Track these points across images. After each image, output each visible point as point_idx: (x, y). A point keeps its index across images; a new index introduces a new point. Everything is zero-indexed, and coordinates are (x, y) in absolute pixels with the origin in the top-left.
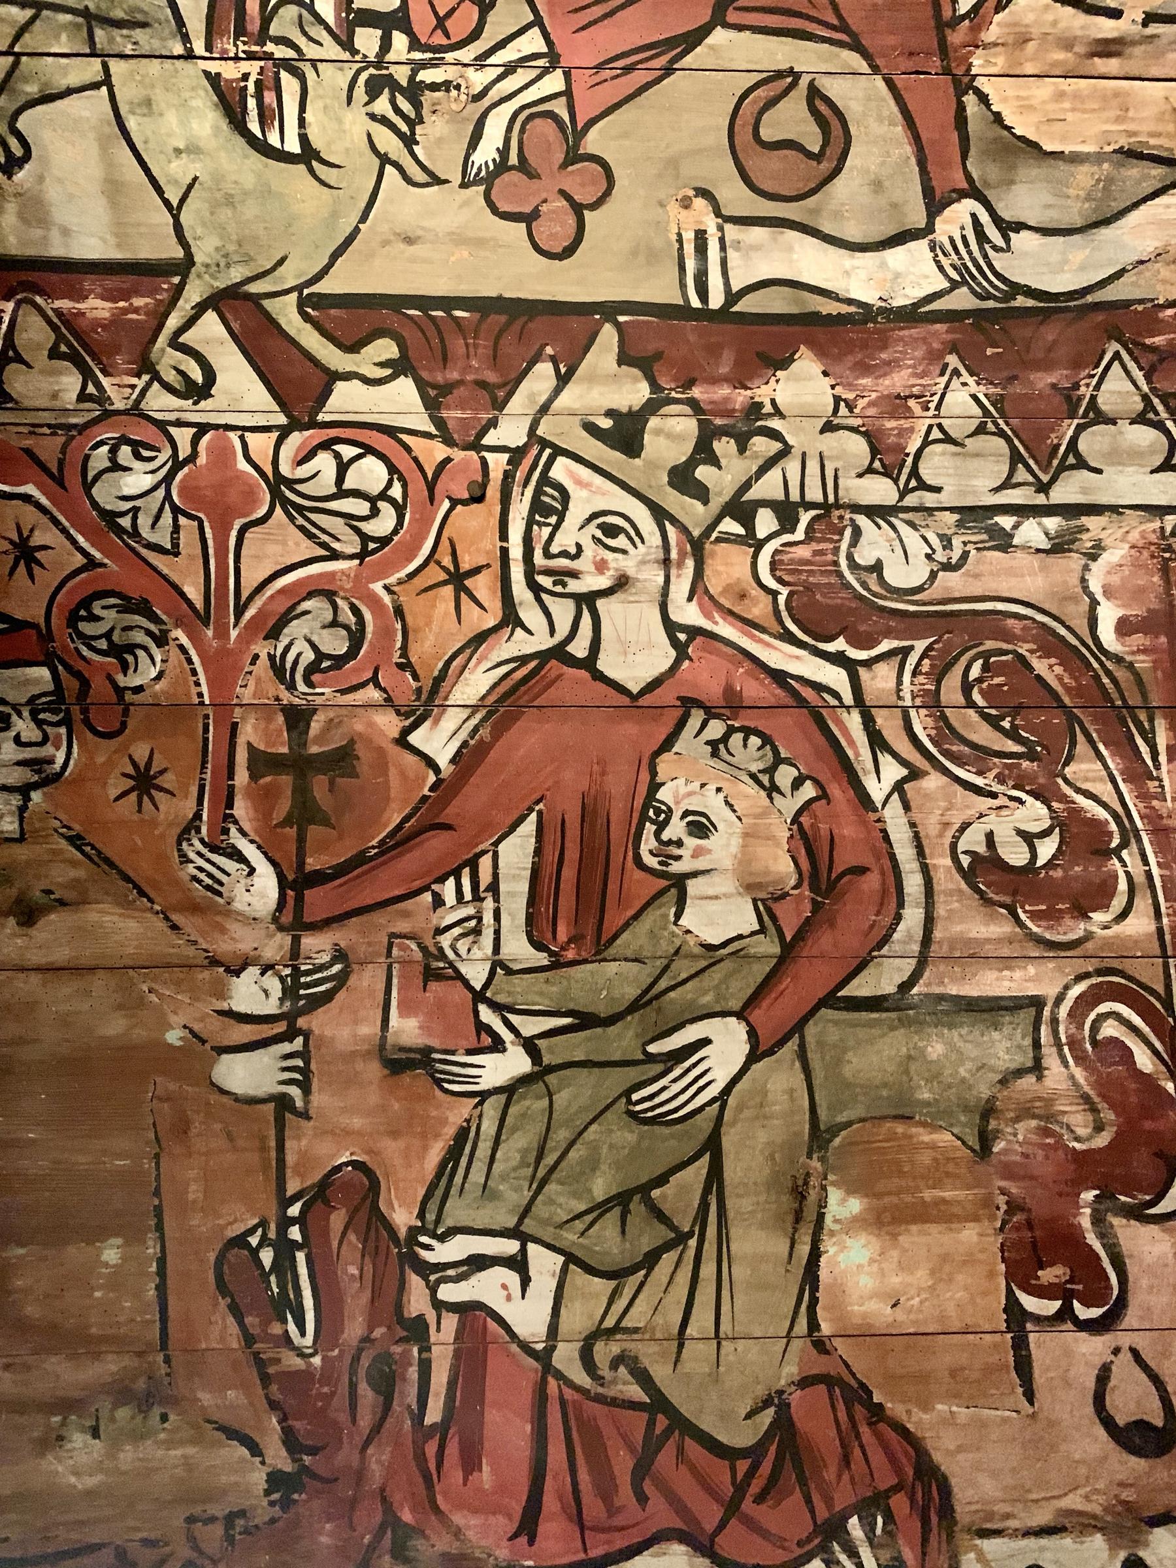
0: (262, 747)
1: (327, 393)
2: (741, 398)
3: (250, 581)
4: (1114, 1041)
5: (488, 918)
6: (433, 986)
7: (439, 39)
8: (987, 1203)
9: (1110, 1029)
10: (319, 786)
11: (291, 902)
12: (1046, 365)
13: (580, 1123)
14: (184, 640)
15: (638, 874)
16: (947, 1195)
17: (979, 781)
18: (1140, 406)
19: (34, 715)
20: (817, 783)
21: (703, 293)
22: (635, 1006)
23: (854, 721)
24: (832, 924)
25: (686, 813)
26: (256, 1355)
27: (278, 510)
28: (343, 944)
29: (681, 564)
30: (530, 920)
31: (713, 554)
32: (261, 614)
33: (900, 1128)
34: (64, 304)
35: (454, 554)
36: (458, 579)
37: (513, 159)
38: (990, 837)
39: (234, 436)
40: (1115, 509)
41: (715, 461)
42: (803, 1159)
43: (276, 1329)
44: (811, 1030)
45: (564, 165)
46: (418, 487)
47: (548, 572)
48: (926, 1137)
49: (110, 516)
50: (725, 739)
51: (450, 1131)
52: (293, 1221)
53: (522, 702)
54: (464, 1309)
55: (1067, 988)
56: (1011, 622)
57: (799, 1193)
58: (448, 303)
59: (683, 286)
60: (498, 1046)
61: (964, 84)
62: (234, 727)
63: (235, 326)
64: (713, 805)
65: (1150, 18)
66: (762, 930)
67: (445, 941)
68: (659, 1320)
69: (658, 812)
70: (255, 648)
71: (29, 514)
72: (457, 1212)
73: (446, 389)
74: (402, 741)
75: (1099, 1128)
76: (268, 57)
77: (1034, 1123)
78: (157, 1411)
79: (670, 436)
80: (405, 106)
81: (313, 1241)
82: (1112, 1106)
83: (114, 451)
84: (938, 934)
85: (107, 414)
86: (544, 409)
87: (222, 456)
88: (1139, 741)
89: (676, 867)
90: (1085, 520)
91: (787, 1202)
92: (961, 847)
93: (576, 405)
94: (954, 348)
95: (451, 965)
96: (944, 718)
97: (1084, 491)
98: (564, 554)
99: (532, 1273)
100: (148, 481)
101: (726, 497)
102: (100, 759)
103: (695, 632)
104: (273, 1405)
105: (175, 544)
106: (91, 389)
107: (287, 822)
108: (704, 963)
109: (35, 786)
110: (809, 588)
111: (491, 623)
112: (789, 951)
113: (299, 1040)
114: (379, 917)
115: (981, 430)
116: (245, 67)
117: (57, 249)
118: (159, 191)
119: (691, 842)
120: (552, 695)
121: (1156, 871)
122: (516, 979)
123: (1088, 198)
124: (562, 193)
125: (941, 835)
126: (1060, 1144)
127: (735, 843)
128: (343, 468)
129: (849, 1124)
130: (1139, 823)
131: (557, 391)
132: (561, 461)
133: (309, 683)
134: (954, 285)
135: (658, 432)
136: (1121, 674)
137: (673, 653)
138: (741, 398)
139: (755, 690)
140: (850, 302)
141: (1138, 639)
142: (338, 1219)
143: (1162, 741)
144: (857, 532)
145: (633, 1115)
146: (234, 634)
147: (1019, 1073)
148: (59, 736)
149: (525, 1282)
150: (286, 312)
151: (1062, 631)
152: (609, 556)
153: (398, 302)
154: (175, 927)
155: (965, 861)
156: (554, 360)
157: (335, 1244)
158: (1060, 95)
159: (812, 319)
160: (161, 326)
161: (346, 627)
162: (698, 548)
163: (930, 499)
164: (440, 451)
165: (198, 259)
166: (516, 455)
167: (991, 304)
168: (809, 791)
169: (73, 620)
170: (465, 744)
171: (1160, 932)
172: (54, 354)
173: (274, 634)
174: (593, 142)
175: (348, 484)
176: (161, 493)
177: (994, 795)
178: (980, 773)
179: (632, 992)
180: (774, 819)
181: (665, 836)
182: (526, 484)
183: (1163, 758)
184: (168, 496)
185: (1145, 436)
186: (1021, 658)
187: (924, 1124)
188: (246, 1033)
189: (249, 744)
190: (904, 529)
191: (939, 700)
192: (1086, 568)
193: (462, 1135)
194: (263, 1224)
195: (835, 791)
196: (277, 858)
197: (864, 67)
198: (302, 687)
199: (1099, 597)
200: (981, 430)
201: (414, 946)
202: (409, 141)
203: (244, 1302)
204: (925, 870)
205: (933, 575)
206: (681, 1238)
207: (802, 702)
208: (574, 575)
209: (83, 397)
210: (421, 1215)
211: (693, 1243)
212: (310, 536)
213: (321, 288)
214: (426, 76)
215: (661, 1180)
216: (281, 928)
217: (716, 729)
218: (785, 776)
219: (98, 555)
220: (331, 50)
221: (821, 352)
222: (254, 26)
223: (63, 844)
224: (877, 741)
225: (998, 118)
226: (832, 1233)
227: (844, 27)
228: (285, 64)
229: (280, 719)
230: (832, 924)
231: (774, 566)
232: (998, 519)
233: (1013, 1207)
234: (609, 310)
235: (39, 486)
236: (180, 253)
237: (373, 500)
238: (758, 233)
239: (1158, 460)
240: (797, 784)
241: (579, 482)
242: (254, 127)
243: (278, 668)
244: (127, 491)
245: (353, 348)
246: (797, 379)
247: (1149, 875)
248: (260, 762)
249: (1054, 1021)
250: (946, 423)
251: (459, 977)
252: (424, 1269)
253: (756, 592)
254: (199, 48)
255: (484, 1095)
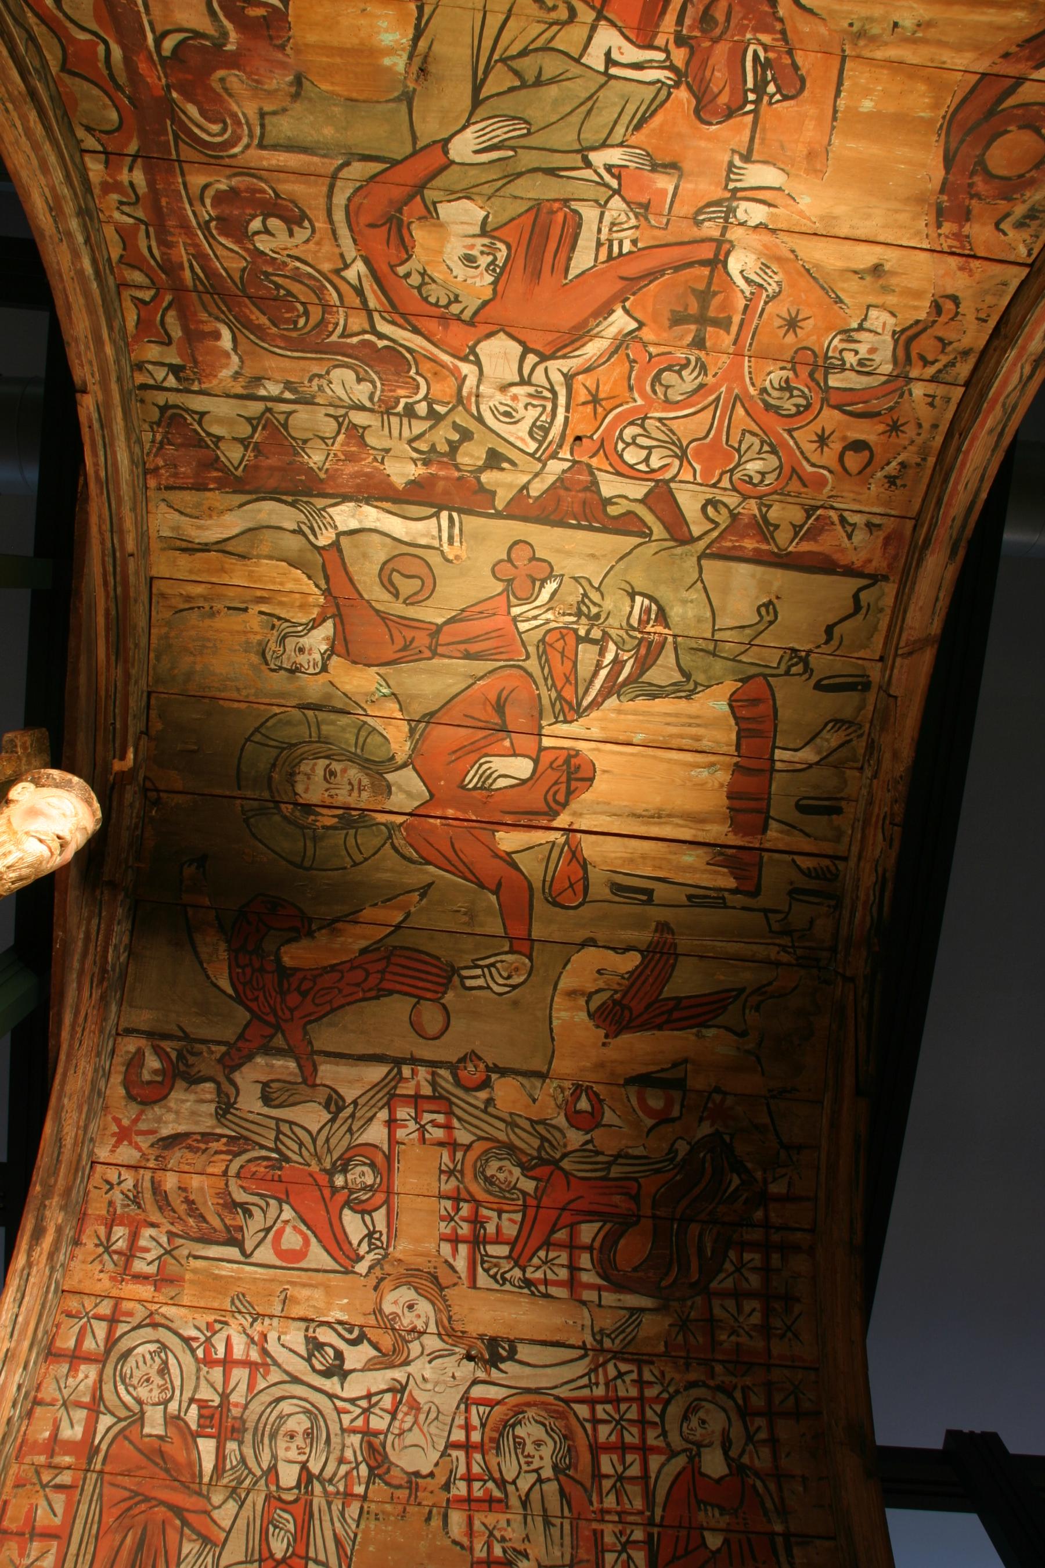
0: (722, 332)
1: (647, 495)
2: (433, 470)
3: (708, 414)
4: (214, 122)
5: (605, 230)
6: (644, 200)
7: (565, 631)
8: (298, 51)
9: (215, 128)
10: (694, 308)
11: (722, 253)
12: (272, 469)
13: (562, 123)
14: (751, 390)
15: (510, 240)
16: (325, 59)
17: (298, 264)
18: (220, 444)
19: (844, 364)
20: (396, 274)
21: (451, 519)
22: (520, 175)
23: (372, 303)
24: (391, 202)
25: (477, 267)
26: (787, 43)
27: (685, 444)
28: (695, 229)
29: (470, 394)
30: (579, 226)
31: (451, 396)
32: (706, 397)
33: (354, 95)
34: (764, 547)
35: (595, 413)
36: (595, 400)
37: (538, 584)
38: (291, 234)
39: (699, 480)
40: (228, 396)
41: (449, 442)
42: (419, 89)
43: (771, 55)
44: (409, 150)
45: (513, 580)
46: (609, 447)
47: (545, 398)
48: (337, 89)
49: (774, 451)
50: (450, 303)
51: (646, 129)
52: (752, 102)
53: (567, 336)
54: (651, 47)
55: (243, 152)
56: (282, 345)
57: (423, 71)
58: (579, 527)
59: (461, 523)
60: (609, 168)
61: (327, 592)
62: (735, 344)
63: (685, 529)
64: (460, 271)
65: (246, 610)
66: (434, 203)
67: (633, 222)
68: (523, 24)
69: (494, 270)
70: (714, 380)
71: (814, 459)
72: (649, 92)
73: (586, 489)
74: (641, 325)
75: (222, 80)
76: (641, 632)
77: (266, 87)
78: (855, 29)
79: (472, 456)
80: (584, 609)
81: (741, 93)
82: (213, 90)
83: (762, 481)
84: (325, 189)
85: (760, 498)
86: (536, 475)
87: (707, 472)
88: (201, 275)
89: (486, 241)
90: (245, 392)
91: (432, 68)
92: (309, 232)
93: (520, 475)
94: (322, 481)
95: (632, 210)
96: (319, 298)
97: (246, 406)
98: (534, 406)
99: (603, 58)
100: (749, 466)
101: (443, 424)
102: (814, 338)
103: (465, 359)
104: (781, 20)
105: (743, 434)
106: (764, 510)
107: (715, 294)
108: (474, 190)
109: (854, 330)
110: (398, 373)
111: (580, 377)
112: (420, 189)
113: (731, 186)
114: (671, 239)
115: (305, 441)
116: (653, 630)
117: (759, 570)
118: (705, 588)
119: (475, 252)
120: (550, 337)
121: (187, 206)
122: (593, 197)
123: (261, 541)
124: (516, 567)
125: (321, 239)
126: (249, 75)
127: (448, 248)
128: (647, 460)
129: (387, 101)
130: (199, 233)
131: (529, 482)
132: (531, 450)
133: (689, 361)
134: (324, 509)
135: (478, 458)
136: (216, 311)
137: (478, 350)
138: (433, 470)
139: (433, 326)
140: (376, 507)
141: (207, 328)
142: (724, 99)
143: (187, 274)
144: (371, 398)
145: (526, 122)
146: (723, 389)
147: (274, 113)
148: (834, 351)
149: (608, 54)
150: (658, 531)
151: (252, 337)
152: (509, 402)
153: (604, 530)
154: (793, 251)
155: (306, 224)
156: (529, 496)
157: (727, 89)
158: (282, 584)
159: (395, 501)
160: (721, 533)
161: (661, 384)
162: (460, 400)
163: (331, 411)
164: (594, 462)
165: (695, 559)
166: (554, 456)
167: (305, 499)
168: (401, 270)
169: (808, 407)
170: (605, 319)
171: (183, 175)
172: (777, 527)
173: (702, 386)
174: (500, 587)
175: (645, 452)
176: (743, 460)
177: (289, 256)
178: (298, 268)
179: (519, 182)
180: (423, 259)
181: (490, 258)
182: (551, 443)
183: (186, 265)
184: (740, 457)
185: (217, 430)
186: (275, 325)
187: (338, 95)
188: (760, 195)
189: (728, 333)
190: (345, 397)
191: (530, 935)
192: (241, 368)
193: (638, 127)
194: (770, 104)
195: (385, 268)
196: (725, 275)
197: (374, 604)
198: (693, 359)
199: (232, 353)
200: (305, 441)
201: (653, 222)
202: (585, 595)
203: (790, 71)
204: (331, 221)
205: (328, 373)
206: (503, 60)
207: (403, 315)
208: (530, 395)
209: (769, 507)
210: (669, 94)
211: (496, 57)
212: (671, 430)
213: (639, 540)
214: (573, 619)
215: (512, 90)
216: (731, 242)
217: (455, 309)
218: (415, 280)
219: (786, 435)
220: (613, 632)
221: (391, 486)
222: (644, 644)
223: (846, 301)
224: (360, 292)
225: (310, 578)
226: (403, 50)
227: (383, 618)
228: (634, 629)
229: (708, 344)
230: (391, 202)
231: (418, 387)
232: (293, 397)
233: (282, 48)
234: (498, 515)
235: (804, 469)
236: (703, 562)
237: (634, 443)
238: (423, 541)
239: (207, 418)
240: (408, 275)
241: (522, 440)
242: (654, 607)
243: (704, 369)
244: (761, 462)
245: (629, 513)
246: (403, 475)
247: (191, 205)
248: (724, 324)
249: (251, 136)
250: (324, 446)
251: (628, 204)
252: (672, 68)
253: (429, 376)
254: (670, 639)
255: (621, 145)
